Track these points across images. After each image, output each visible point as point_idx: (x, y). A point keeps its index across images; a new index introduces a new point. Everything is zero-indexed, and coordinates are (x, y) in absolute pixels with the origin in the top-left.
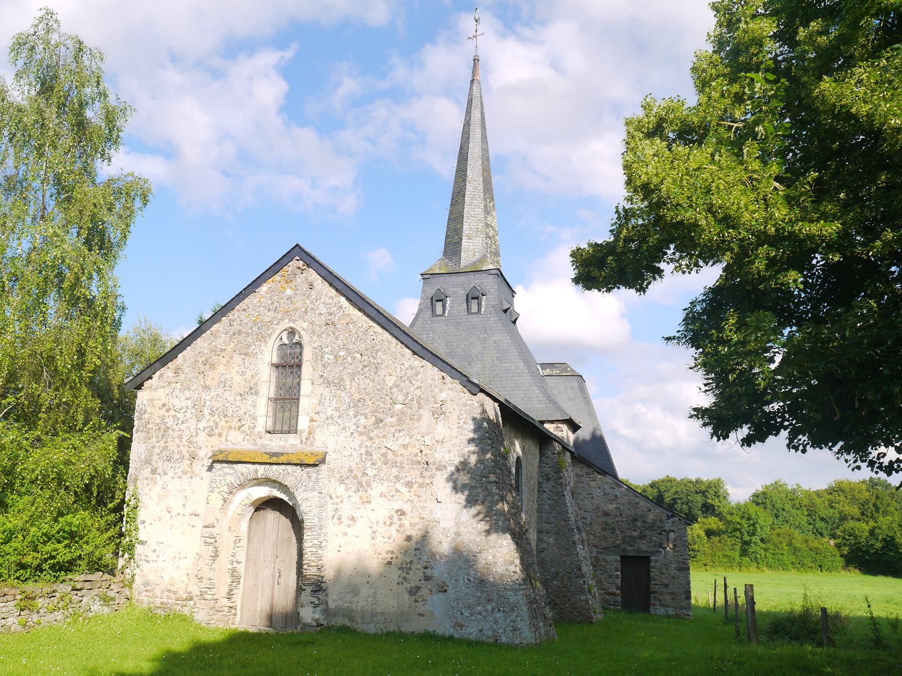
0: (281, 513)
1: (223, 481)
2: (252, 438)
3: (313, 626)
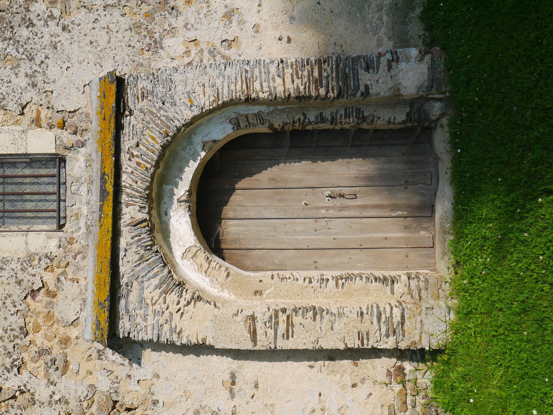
0: (226, 203)
1: (157, 307)
2: (71, 260)
3: (432, 59)
